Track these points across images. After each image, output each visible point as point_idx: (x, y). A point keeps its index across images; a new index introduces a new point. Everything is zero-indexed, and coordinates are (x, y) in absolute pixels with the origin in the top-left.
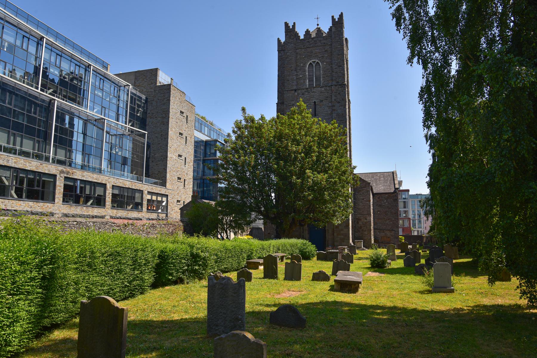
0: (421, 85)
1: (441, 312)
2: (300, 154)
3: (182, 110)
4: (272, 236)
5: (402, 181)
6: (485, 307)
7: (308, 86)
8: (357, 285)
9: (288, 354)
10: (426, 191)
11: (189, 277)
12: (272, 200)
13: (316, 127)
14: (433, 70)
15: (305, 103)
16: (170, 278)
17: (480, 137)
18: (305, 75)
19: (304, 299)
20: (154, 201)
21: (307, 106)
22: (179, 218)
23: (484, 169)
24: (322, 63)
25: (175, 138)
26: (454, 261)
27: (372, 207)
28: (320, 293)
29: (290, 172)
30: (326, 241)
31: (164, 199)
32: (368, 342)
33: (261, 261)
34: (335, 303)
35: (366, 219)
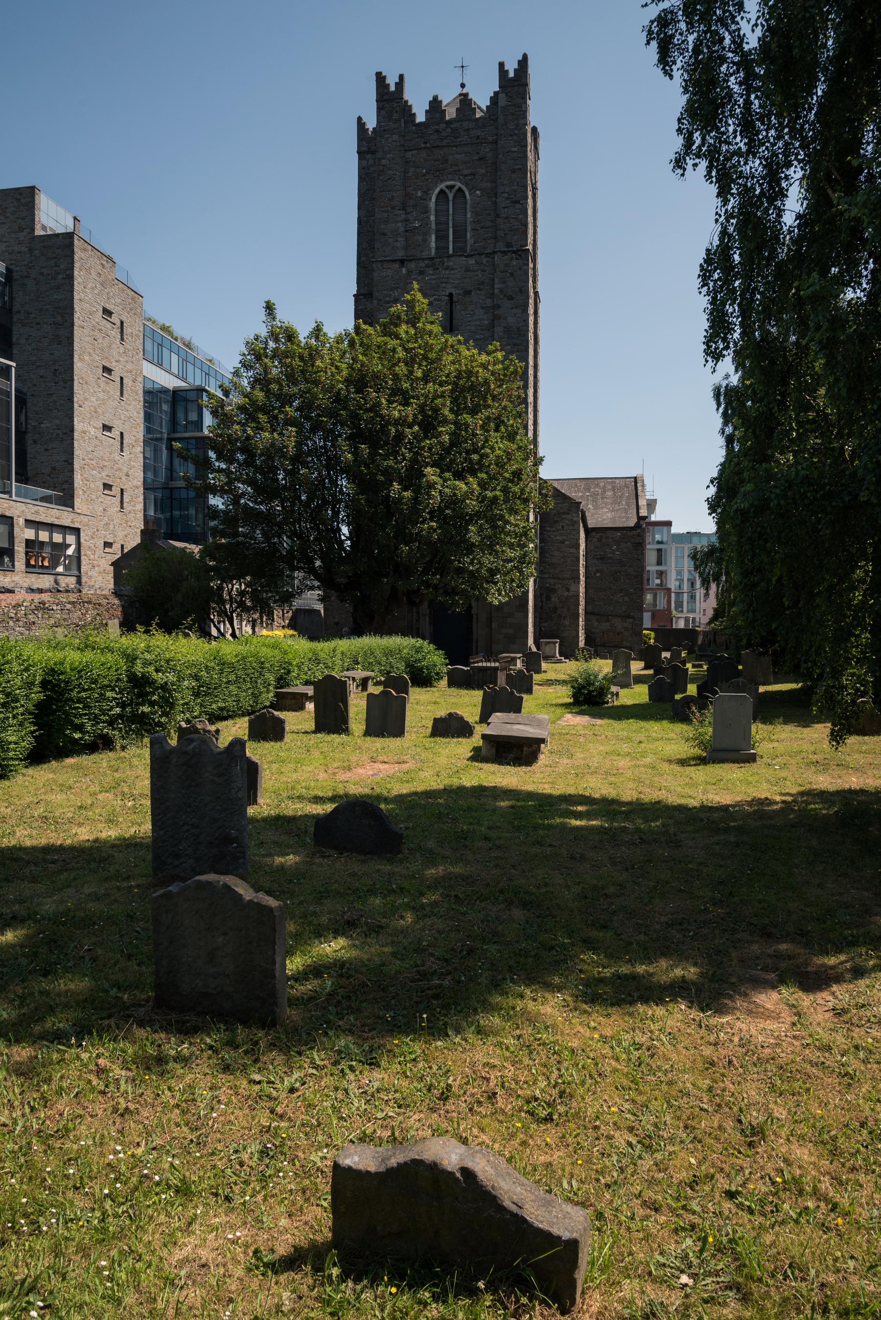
0: (706, 245)
1: (724, 809)
2: (410, 426)
3: (108, 307)
4: (345, 629)
5: (655, 501)
6: (823, 796)
7: (433, 252)
8: (534, 747)
9: (348, 922)
10: (707, 525)
11: (127, 732)
12: (342, 542)
13: (451, 358)
14: (742, 206)
15: (425, 296)
16: (77, 736)
17: (841, 384)
18: (428, 223)
19: (408, 782)
20: (42, 544)
21: (430, 304)
22: (112, 586)
23: (843, 471)
25: (91, 379)
26: (762, 689)
27: (582, 562)
28: (448, 765)
29: (386, 472)
30: (474, 643)
31: (71, 539)
32: (546, 885)
33: (310, 691)
34: (480, 791)
35: (568, 590)
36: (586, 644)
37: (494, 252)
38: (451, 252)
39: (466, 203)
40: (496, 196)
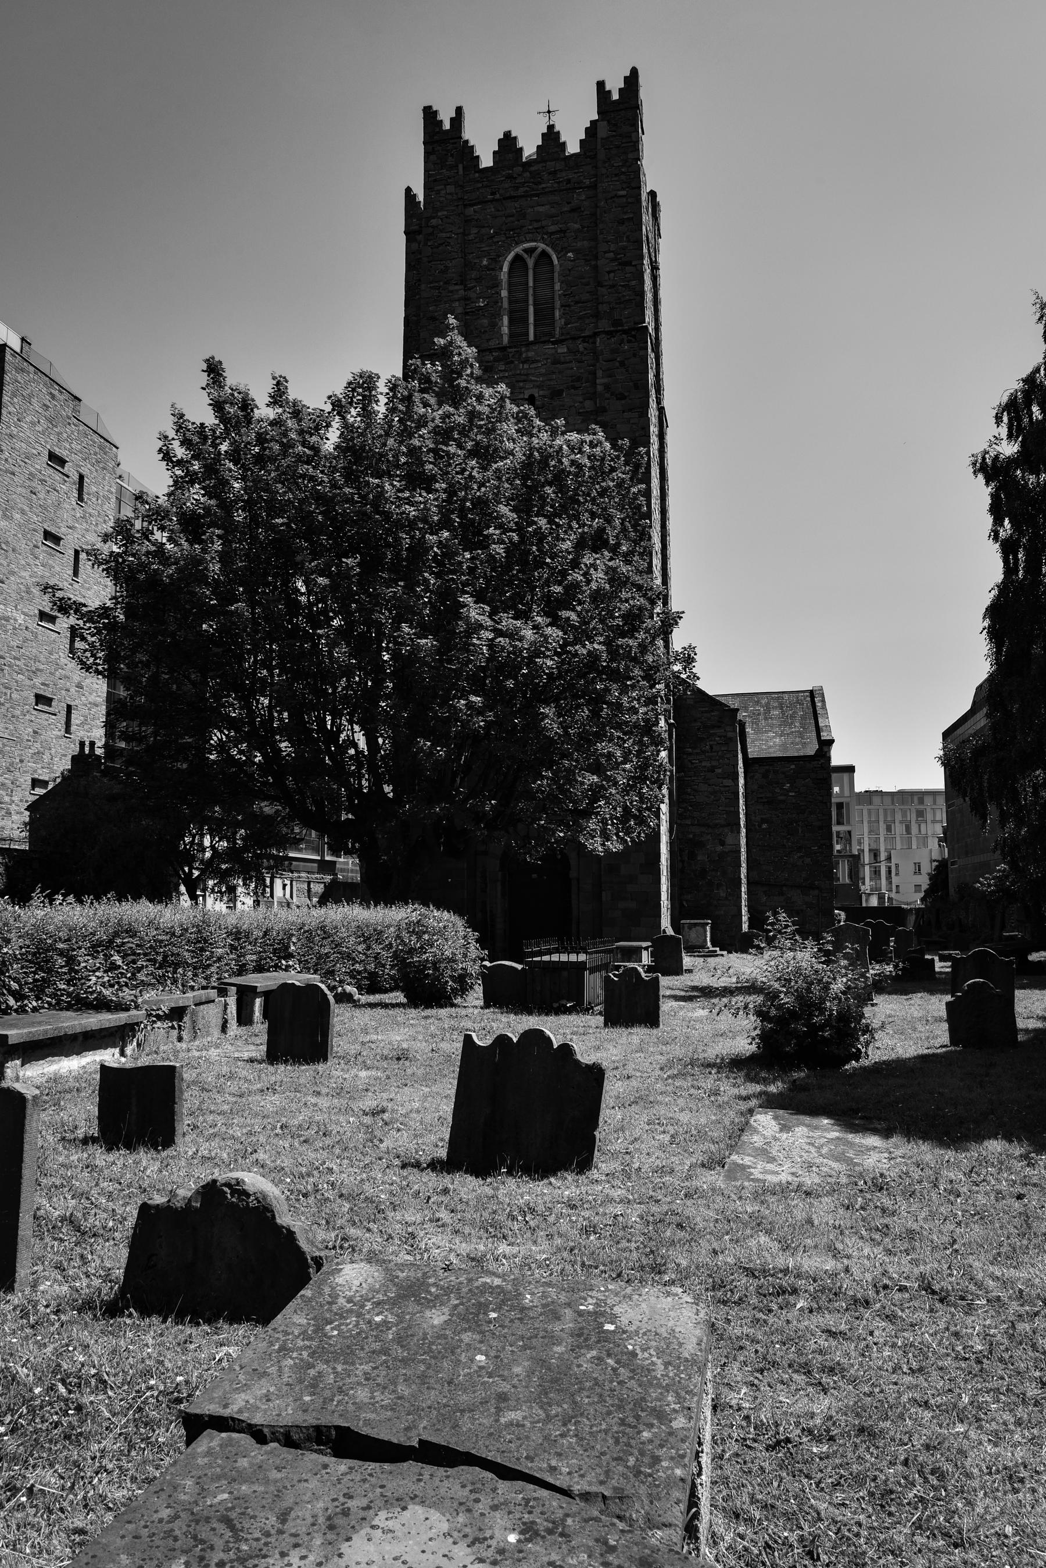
2: (434, 531)
7: (506, 340)
18: (497, 300)
35: (722, 843)
36: (750, 927)
37: (596, 334)
38: (531, 338)
40: (596, 258)
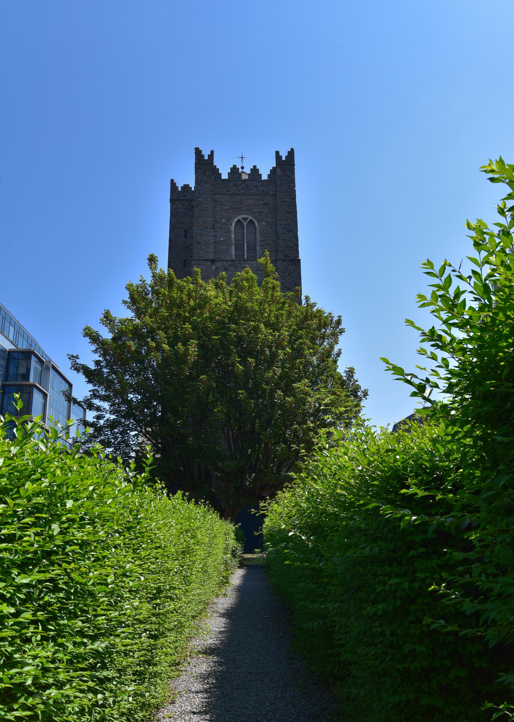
7: (234, 257)
18: (230, 239)
24: (258, 222)
38: (246, 258)
39: (255, 229)
